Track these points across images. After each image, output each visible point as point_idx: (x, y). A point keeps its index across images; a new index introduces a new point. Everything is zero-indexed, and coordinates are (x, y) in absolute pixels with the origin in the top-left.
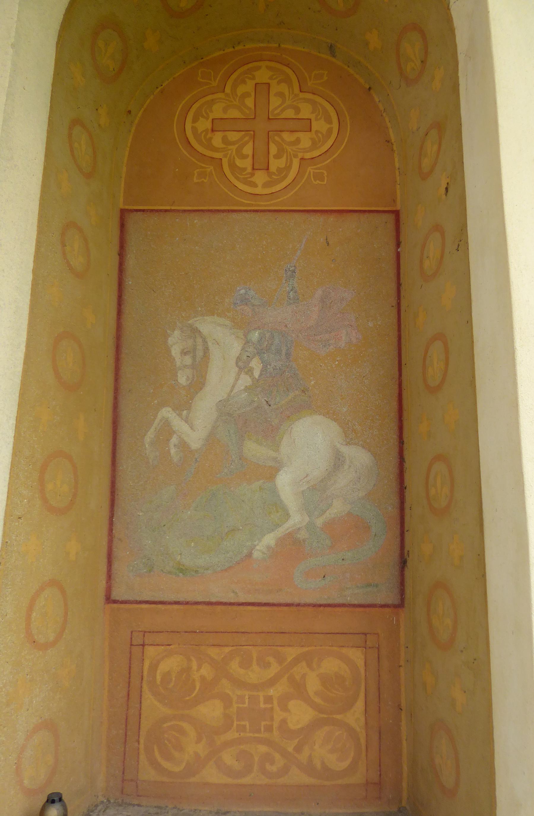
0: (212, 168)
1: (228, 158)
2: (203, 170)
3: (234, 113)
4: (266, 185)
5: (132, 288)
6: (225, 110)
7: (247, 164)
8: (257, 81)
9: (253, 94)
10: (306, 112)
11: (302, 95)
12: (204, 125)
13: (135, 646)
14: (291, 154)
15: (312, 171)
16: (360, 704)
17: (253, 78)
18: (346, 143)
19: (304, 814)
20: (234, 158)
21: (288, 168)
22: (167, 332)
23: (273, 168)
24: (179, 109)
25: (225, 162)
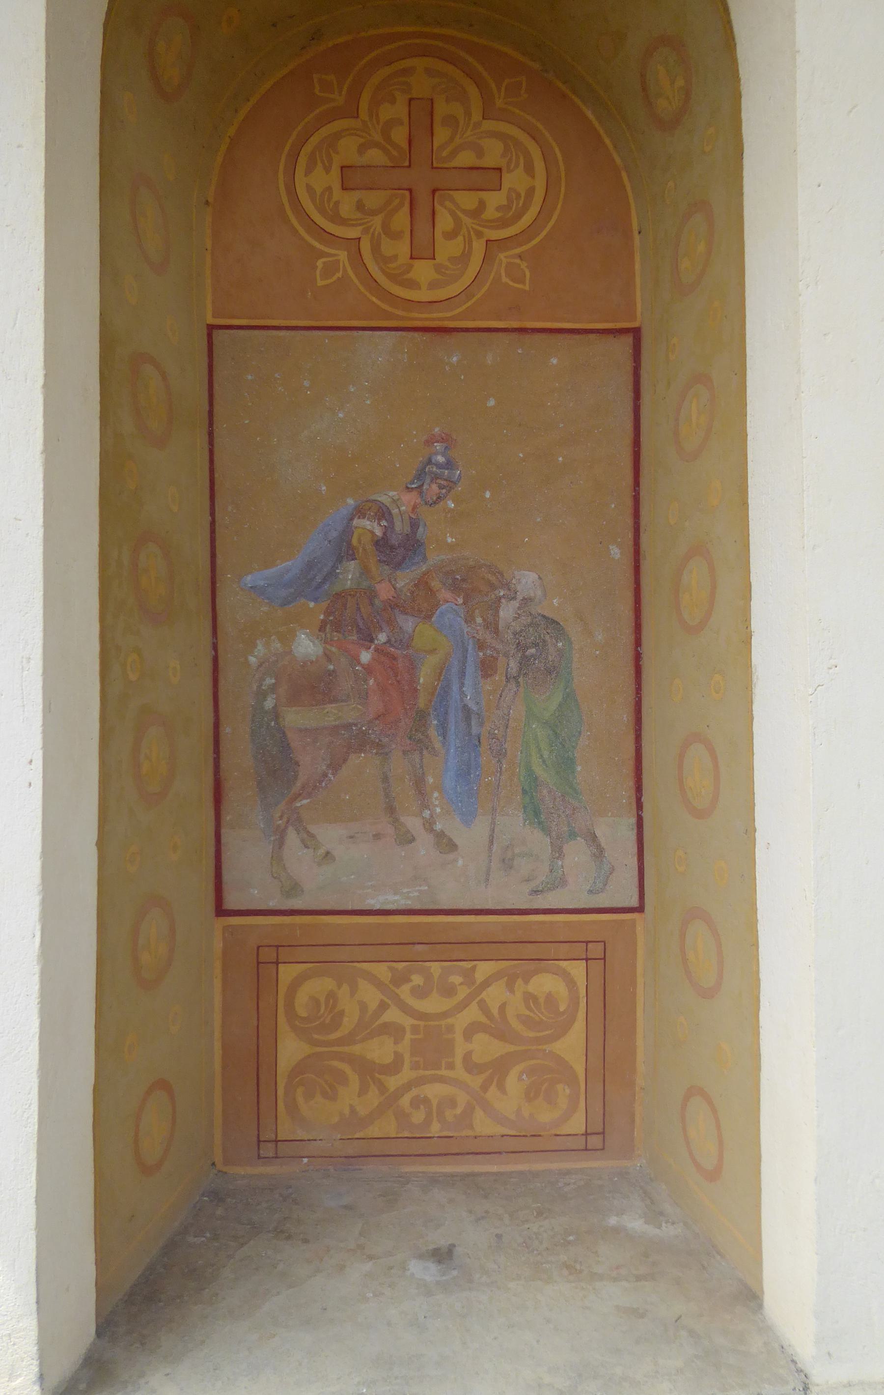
2: (330, 259)
6: (362, 149)
7: (403, 249)
9: (406, 120)
10: (494, 153)
11: (488, 125)
14: (468, 243)
15: (504, 261)
16: (579, 1025)
18: (563, 160)
19: (280, 849)
21: (465, 258)
22: (539, 1279)
25: (366, 247)
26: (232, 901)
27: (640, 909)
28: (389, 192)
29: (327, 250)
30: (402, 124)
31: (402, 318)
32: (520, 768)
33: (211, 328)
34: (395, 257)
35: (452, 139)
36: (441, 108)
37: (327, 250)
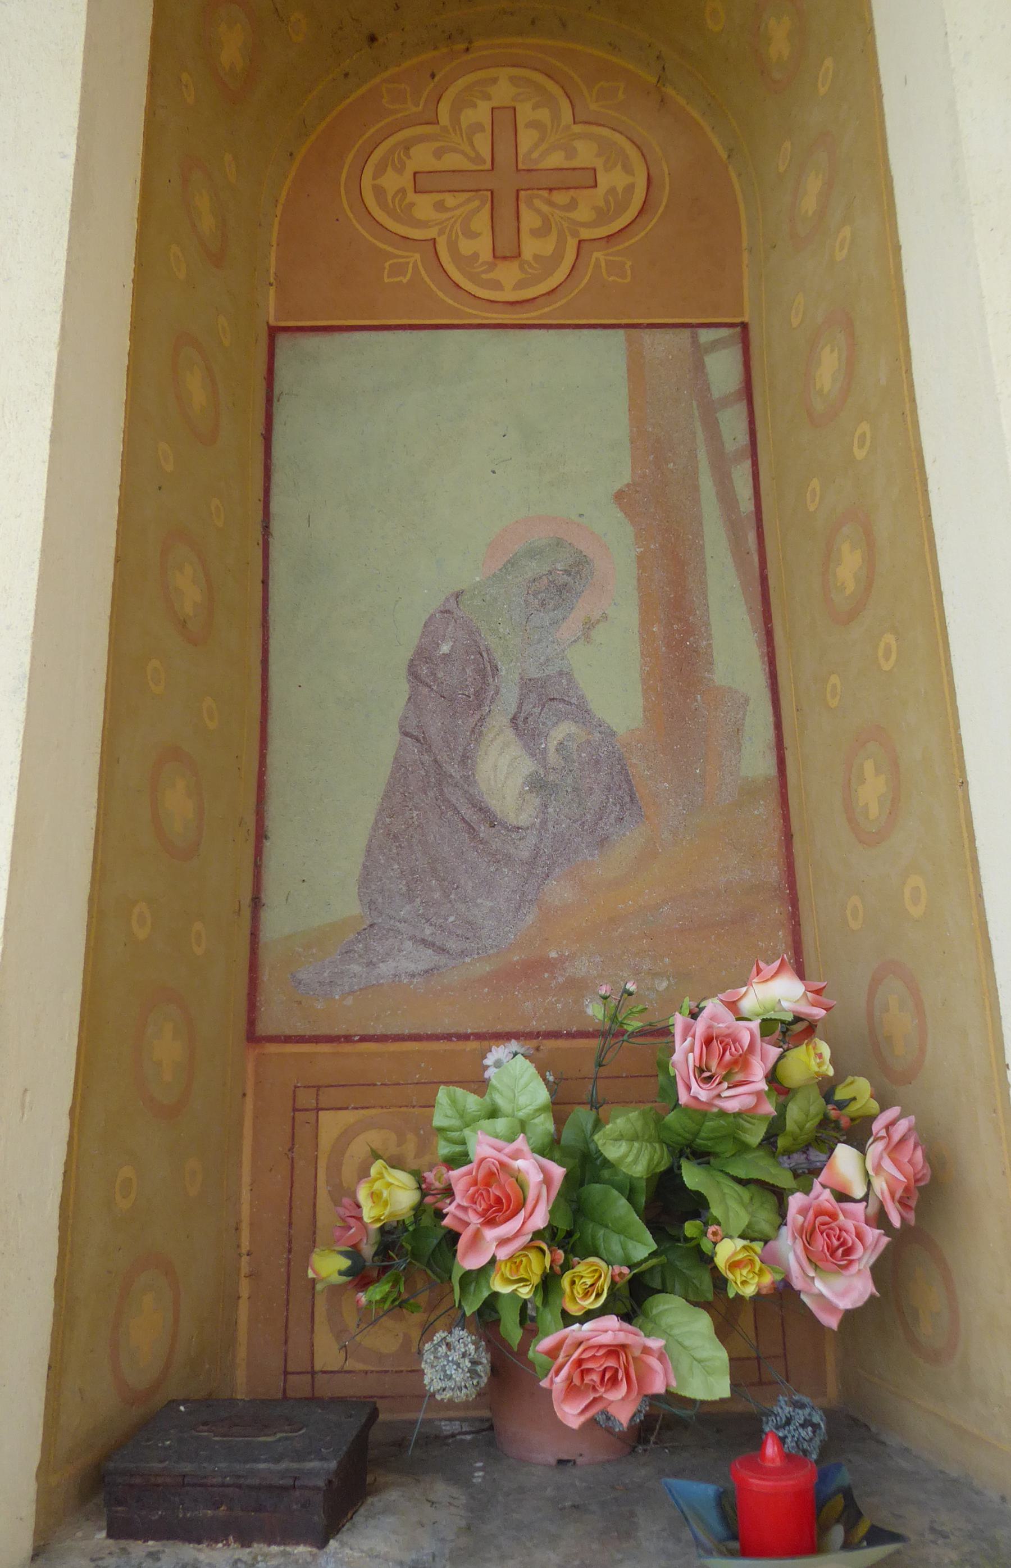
0: (417, 256)
1: (446, 234)
3: (452, 161)
4: (520, 285)
5: (442, 5)
6: (438, 154)
7: (483, 247)
8: (495, 104)
10: (586, 154)
12: (392, 181)
13: (293, 1144)
17: (488, 97)
20: (457, 236)
23: (527, 253)
24: (427, 279)
26: (269, 1023)
27: (273, 332)
28: (541, 166)
29: (397, 252)
30: (483, 130)
31: (476, 317)
32: (542, 709)
33: (273, 332)
34: (476, 256)
35: (542, 139)
36: (526, 112)
37: (397, 252)
